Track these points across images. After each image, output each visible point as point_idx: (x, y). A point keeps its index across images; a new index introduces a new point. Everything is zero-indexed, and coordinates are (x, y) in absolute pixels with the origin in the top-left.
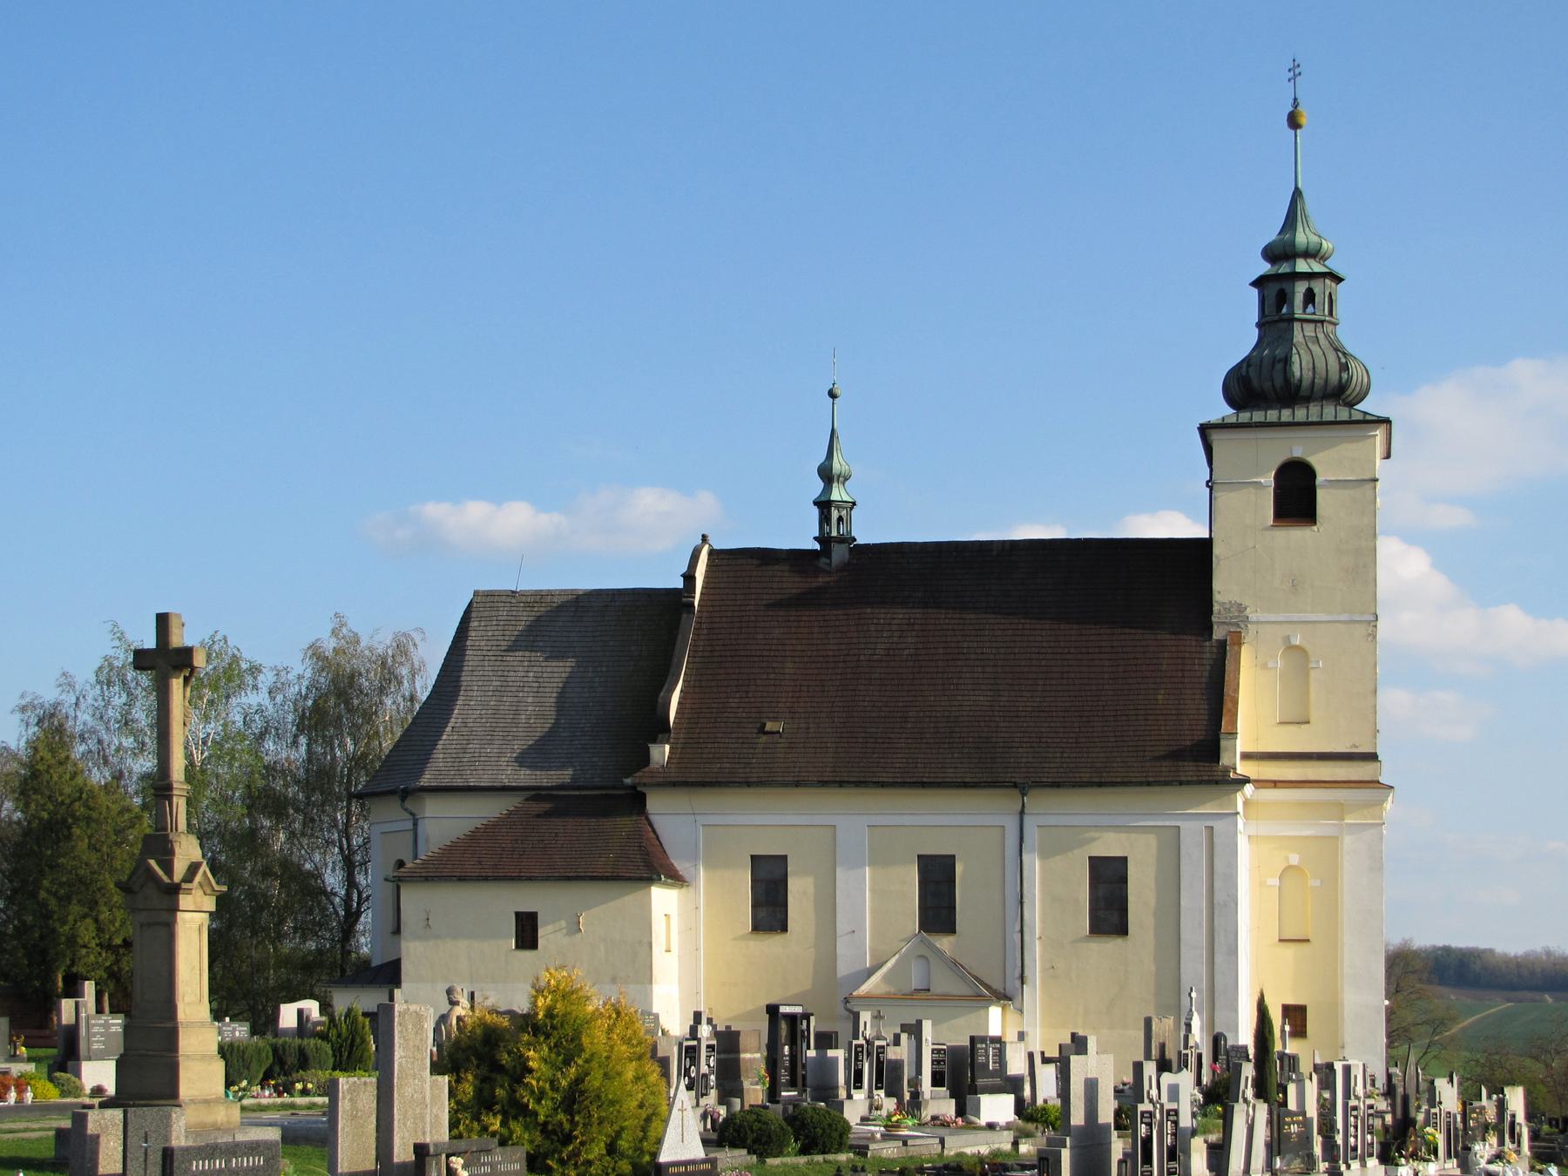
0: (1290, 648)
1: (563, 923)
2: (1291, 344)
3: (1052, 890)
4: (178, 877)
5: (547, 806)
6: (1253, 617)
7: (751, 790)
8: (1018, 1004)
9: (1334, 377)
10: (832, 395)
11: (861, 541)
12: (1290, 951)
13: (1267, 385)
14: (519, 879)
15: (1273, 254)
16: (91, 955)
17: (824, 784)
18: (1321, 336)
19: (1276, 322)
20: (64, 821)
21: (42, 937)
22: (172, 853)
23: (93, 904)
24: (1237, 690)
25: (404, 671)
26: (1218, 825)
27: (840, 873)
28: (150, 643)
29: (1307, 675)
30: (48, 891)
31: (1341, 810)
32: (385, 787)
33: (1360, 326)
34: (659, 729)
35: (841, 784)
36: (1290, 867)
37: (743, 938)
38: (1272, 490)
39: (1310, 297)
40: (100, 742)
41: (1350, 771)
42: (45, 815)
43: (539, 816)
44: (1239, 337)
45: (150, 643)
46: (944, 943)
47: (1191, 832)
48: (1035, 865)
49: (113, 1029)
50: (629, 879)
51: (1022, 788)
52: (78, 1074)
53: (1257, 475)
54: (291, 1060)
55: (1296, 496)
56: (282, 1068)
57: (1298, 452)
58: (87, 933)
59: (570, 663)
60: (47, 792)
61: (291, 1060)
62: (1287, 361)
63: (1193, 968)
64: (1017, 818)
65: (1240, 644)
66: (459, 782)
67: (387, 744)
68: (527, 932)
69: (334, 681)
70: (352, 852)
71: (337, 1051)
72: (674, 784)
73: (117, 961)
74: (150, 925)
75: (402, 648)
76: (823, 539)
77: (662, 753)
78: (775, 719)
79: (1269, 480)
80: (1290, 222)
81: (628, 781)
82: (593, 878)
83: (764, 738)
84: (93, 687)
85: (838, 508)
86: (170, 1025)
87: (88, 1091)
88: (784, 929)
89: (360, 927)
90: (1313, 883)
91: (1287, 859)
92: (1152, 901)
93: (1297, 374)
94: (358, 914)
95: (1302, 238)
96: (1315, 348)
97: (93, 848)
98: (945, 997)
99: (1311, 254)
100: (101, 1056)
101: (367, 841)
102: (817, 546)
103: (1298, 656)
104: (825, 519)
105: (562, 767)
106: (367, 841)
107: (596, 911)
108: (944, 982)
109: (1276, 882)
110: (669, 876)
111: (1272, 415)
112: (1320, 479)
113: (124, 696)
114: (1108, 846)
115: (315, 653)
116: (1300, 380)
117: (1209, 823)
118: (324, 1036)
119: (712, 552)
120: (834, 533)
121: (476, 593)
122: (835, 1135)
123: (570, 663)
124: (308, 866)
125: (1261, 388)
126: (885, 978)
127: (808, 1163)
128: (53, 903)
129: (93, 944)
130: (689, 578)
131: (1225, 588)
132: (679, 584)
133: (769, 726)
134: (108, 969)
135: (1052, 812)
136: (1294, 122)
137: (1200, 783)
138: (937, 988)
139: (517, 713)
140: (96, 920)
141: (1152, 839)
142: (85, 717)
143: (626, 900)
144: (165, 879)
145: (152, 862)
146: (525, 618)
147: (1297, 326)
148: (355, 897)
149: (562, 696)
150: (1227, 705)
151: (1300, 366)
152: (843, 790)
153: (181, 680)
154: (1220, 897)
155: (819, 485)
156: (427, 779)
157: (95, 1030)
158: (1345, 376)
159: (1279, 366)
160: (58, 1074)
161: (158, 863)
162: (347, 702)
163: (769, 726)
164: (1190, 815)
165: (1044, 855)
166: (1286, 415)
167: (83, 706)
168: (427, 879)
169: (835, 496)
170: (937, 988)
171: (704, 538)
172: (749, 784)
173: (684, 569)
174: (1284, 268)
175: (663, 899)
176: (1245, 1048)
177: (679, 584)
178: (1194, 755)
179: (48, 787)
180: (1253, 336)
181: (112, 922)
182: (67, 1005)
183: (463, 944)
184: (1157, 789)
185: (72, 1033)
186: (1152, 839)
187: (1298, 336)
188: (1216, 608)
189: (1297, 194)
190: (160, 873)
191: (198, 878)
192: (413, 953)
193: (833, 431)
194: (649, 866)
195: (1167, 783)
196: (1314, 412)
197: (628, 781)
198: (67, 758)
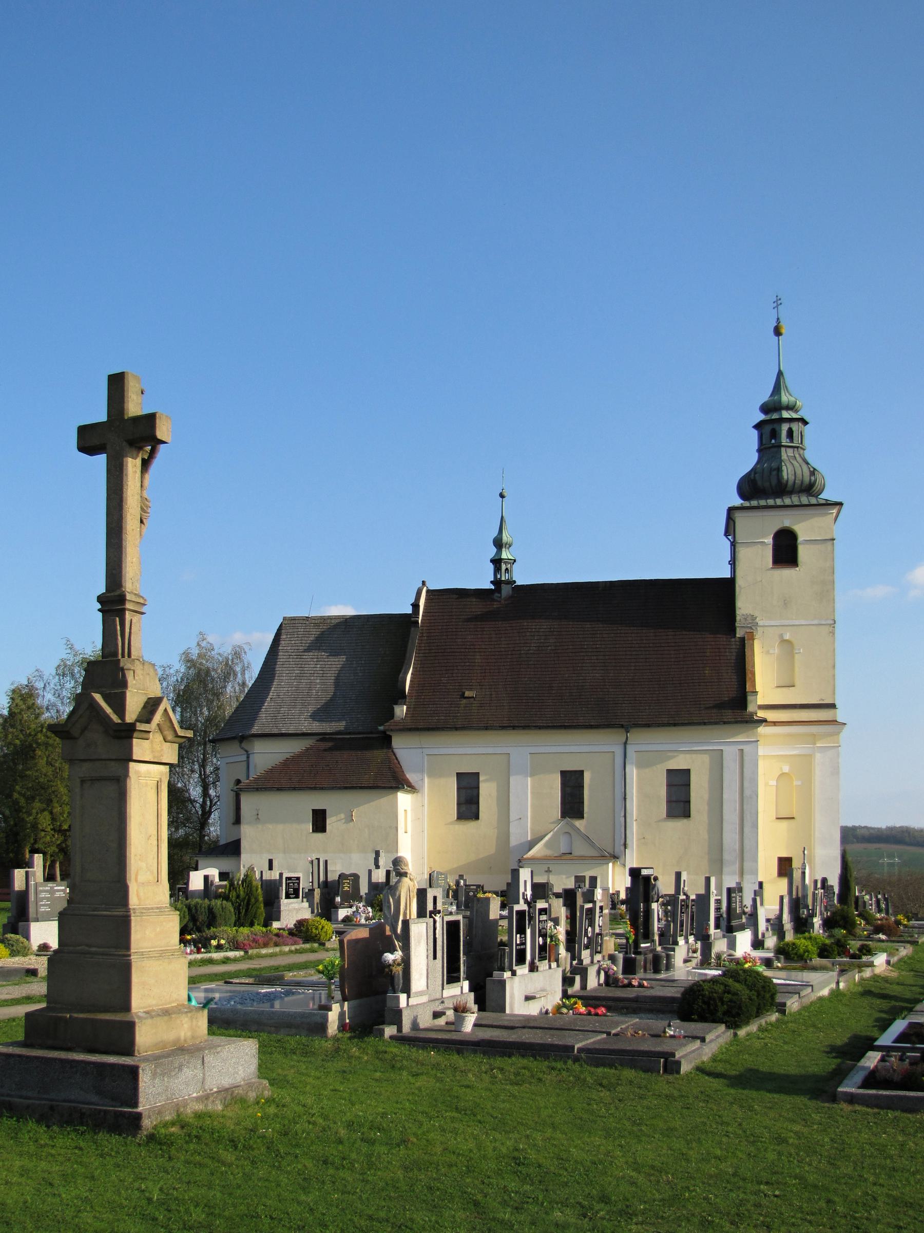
0: (784, 641)
1: (342, 816)
2: (781, 461)
3: (644, 787)
4: (130, 717)
5: (330, 744)
6: (760, 623)
7: (458, 733)
8: (622, 859)
9: (807, 479)
10: (502, 496)
11: (519, 583)
12: (784, 824)
13: (767, 484)
14: (315, 788)
15: (765, 409)
16: (48, 837)
17: (503, 728)
18: (797, 456)
19: (770, 448)
20: (31, 746)
21: (16, 825)
22: (124, 684)
23: (49, 802)
24: (753, 666)
25: (238, 669)
26: (747, 748)
27: (513, 779)
28: (100, 415)
29: (793, 657)
30: (20, 793)
31: (814, 738)
32: (229, 735)
33: (818, 449)
34: (400, 697)
35: (514, 728)
36: (783, 774)
37: (451, 823)
38: (771, 546)
39: (790, 433)
40: (58, 711)
41: (820, 714)
42: (18, 742)
43: (325, 750)
44: (747, 458)
45: (100, 415)
46: (578, 823)
47: (730, 753)
48: (633, 772)
49: (58, 894)
50: (384, 788)
51: (626, 728)
52: (27, 936)
53: (763, 537)
54: (202, 918)
55: (786, 550)
56: (195, 924)
57: (787, 523)
58: (45, 821)
59: (343, 658)
60: (19, 727)
61: (202, 918)
62: (779, 470)
63: (730, 837)
64: (622, 746)
65: (753, 639)
66: (275, 731)
67: (229, 711)
68: (319, 821)
69: (198, 674)
70: (206, 777)
71: (237, 909)
72: (410, 730)
73: (65, 840)
74: (94, 780)
75: (238, 654)
76: (497, 582)
77: (401, 711)
78: (471, 689)
79: (769, 540)
80: (777, 389)
81: (381, 728)
82: (361, 788)
83: (464, 701)
84: (54, 677)
85: (505, 563)
86: (118, 912)
87: (35, 947)
88: (477, 817)
89: (210, 821)
90: (796, 783)
91: (781, 769)
92: (706, 796)
93: (785, 477)
94: (210, 813)
95: (785, 398)
96: (795, 463)
97: (49, 763)
98: (582, 858)
99: (791, 408)
100: (46, 918)
101: (217, 769)
102: (493, 587)
103: (787, 644)
104: (497, 569)
105: (339, 720)
106: (217, 769)
107: (361, 808)
108: (580, 849)
109: (774, 783)
110: (409, 786)
111: (771, 502)
112: (801, 538)
113: (73, 682)
114: (679, 763)
115: (189, 662)
116: (787, 481)
117: (741, 747)
118: (226, 897)
119: (428, 591)
120: (503, 579)
121: (285, 619)
122: (768, 995)
123: (343, 658)
124: (179, 785)
125: (765, 486)
126: (547, 845)
127: (760, 1029)
128: (22, 801)
129: (49, 829)
130: (416, 606)
131: (744, 606)
132: (409, 610)
133: (467, 694)
134: (58, 845)
135: (644, 742)
136: (777, 332)
137: (736, 722)
138: (576, 853)
139: (310, 689)
140: (51, 813)
141: (706, 758)
142: (49, 697)
143: (381, 801)
144: (115, 718)
145: (98, 697)
146: (315, 632)
147: (783, 449)
148: (208, 803)
149: (337, 679)
150: (749, 676)
151: (787, 473)
152: (515, 731)
153: (138, 462)
154: (747, 792)
155: (494, 550)
156: (255, 730)
157: (43, 895)
158: (813, 478)
159: (774, 473)
160: (9, 936)
161: (106, 698)
162: (206, 686)
163: (467, 694)
164: (729, 743)
165: (640, 766)
166: (779, 502)
167: (48, 689)
168: (257, 790)
169: (504, 556)
170: (576, 853)
171: (424, 583)
172: (456, 729)
173: (413, 601)
174: (775, 416)
175: (404, 799)
176: (832, 887)
177: (409, 610)
178: (731, 705)
179: (21, 723)
180: (755, 457)
181: (62, 814)
182: (19, 874)
183: (280, 827)
184: (710, 727)
185: (23, 897)
186: (706, 758)
187: (784, 457)
188: (738, 618)
189: (780, 374)
190: (108, 710)
191: (158, 717)
192: (248, 833)
193: (502, 517)
194: (395, 781)
195: (716, 723)
196: (795, 499)
197: (381, 728)
198: (33, 704)
